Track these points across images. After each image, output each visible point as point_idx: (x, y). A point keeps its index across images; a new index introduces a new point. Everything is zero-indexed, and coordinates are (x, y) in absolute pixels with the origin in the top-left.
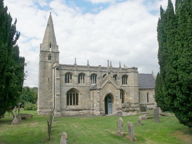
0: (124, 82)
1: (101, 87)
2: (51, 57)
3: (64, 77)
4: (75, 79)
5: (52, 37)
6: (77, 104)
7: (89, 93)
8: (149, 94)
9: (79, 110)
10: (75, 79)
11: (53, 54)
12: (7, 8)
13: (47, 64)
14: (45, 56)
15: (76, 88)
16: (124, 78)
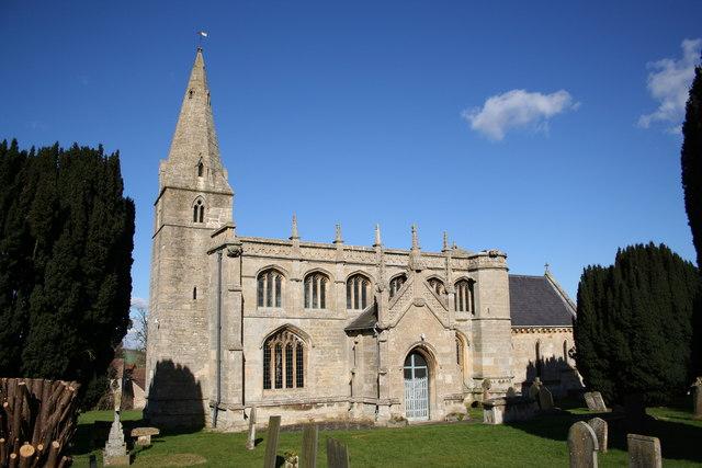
0: (461, 302)
1: (395, 320)
2: (202, 208)
3: (255, 283)
4: (293, 290)
5: (206, 139)
6: (300, 384)
7: (342, 342)
8: (541, 346)
9: (307, 407)
10: (293, 290)
11: (212, 197)
12: (662, 246)
13: (187, 235)
14: (181, 207)
15: (297, 323)
16: (356, 284)
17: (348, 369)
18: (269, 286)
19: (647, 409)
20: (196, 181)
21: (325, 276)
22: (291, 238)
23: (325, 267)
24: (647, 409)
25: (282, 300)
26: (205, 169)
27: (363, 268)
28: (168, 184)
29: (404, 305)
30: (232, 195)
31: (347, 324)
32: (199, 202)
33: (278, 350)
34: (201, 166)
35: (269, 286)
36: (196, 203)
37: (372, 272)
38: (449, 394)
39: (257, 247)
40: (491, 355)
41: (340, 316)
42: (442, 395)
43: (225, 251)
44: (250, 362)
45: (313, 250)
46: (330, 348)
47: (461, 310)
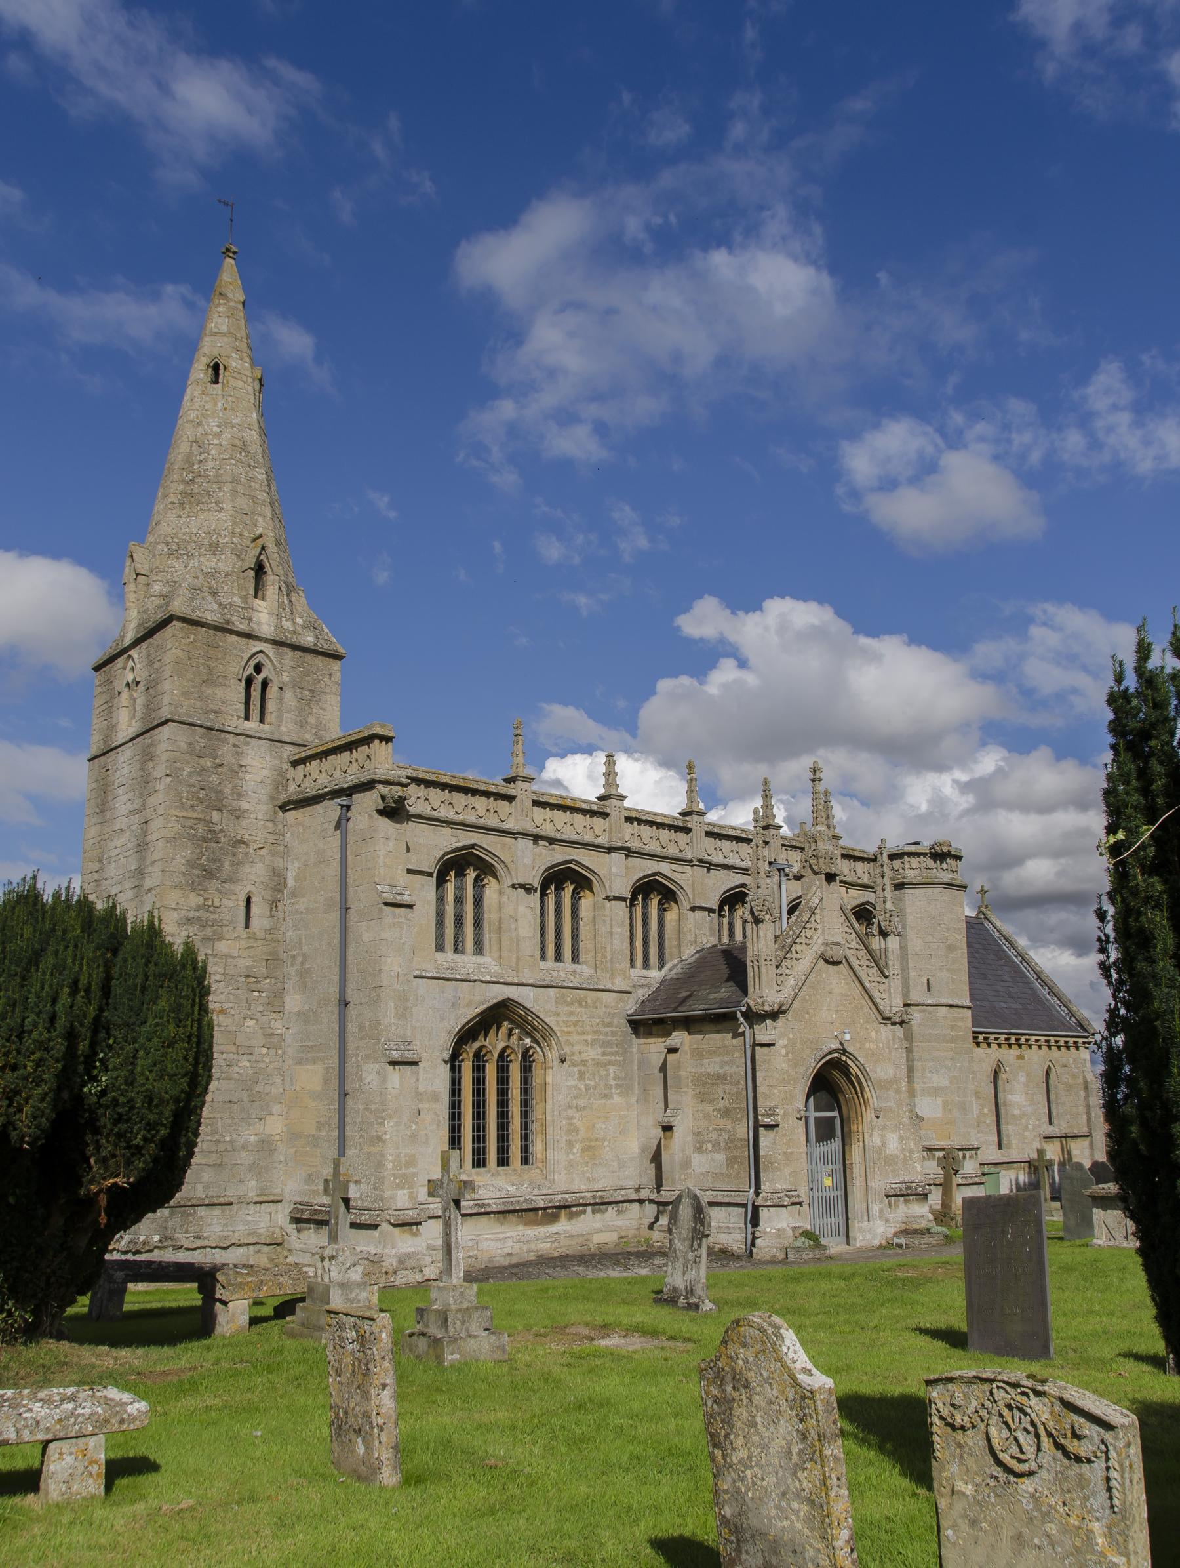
2: (265, 684)
8: (1002, 1076)
17: (653, 1117)
18: (459, 900)
19: (199, 1303)
20: (248, 614)
21: (485, 869)
22: (510, 780)
23: (587, 858)
24: (199, 1303)
25: (489, 937)
26: (270, 579)
27: (665, 868)
28: (178, 606)
29: (805, 959)
30: (338, 657)
31: (631, 1006)
32: (258, 668)
33: (479, 1058)
34: (259, 570)
35: (459, 900)
36: (250, 670)
37: (684, 877)
38: (894, 1181)
39: (436, 795)
40: (936, 1092)
41: (619, 984)
42: (880, 1184)
43: (367, 802)
44: (435, 1098)
45: (558, 814)
46: (598, 1064)
47: (558, 957)
